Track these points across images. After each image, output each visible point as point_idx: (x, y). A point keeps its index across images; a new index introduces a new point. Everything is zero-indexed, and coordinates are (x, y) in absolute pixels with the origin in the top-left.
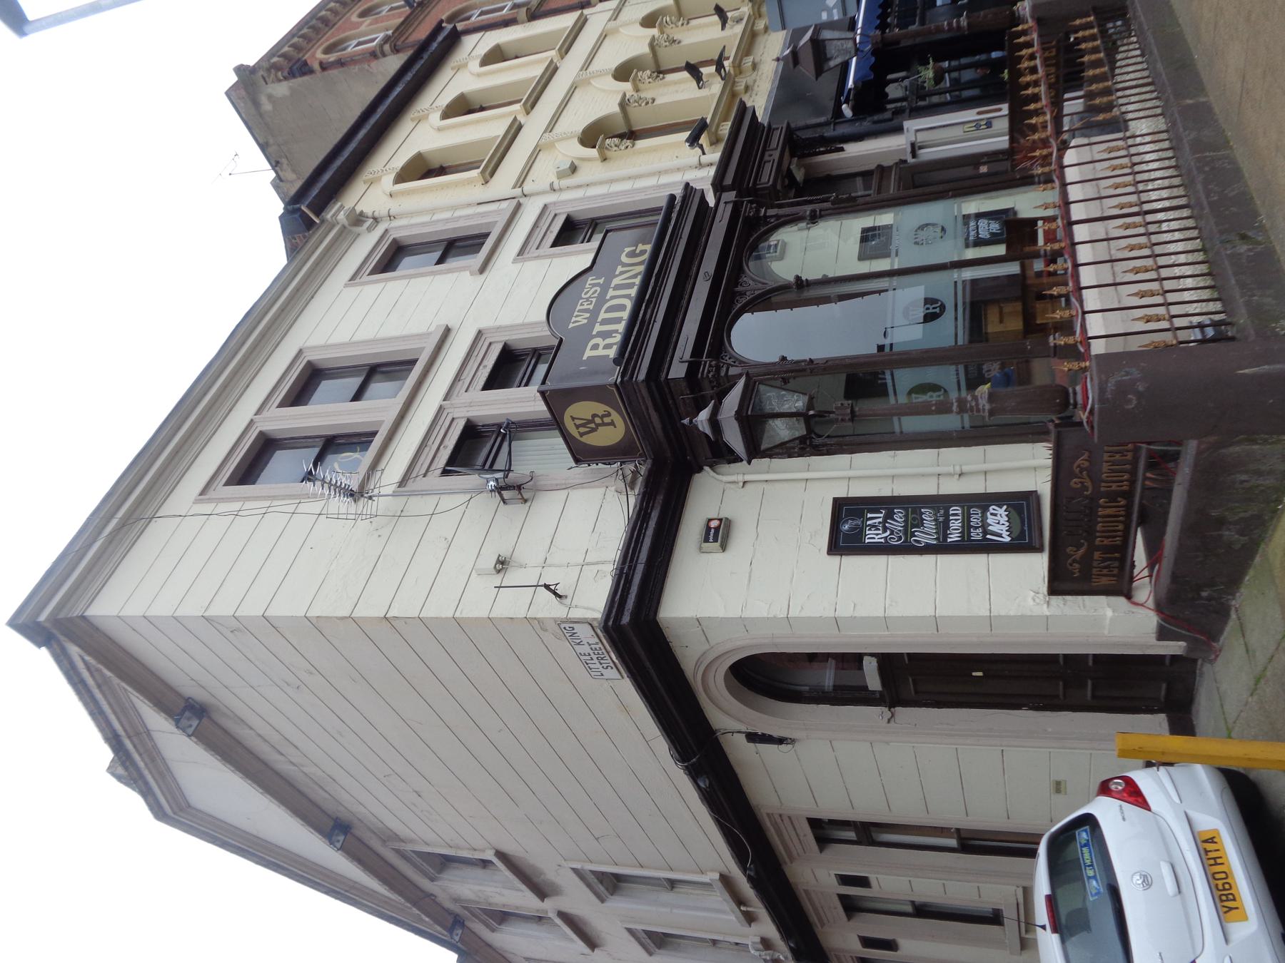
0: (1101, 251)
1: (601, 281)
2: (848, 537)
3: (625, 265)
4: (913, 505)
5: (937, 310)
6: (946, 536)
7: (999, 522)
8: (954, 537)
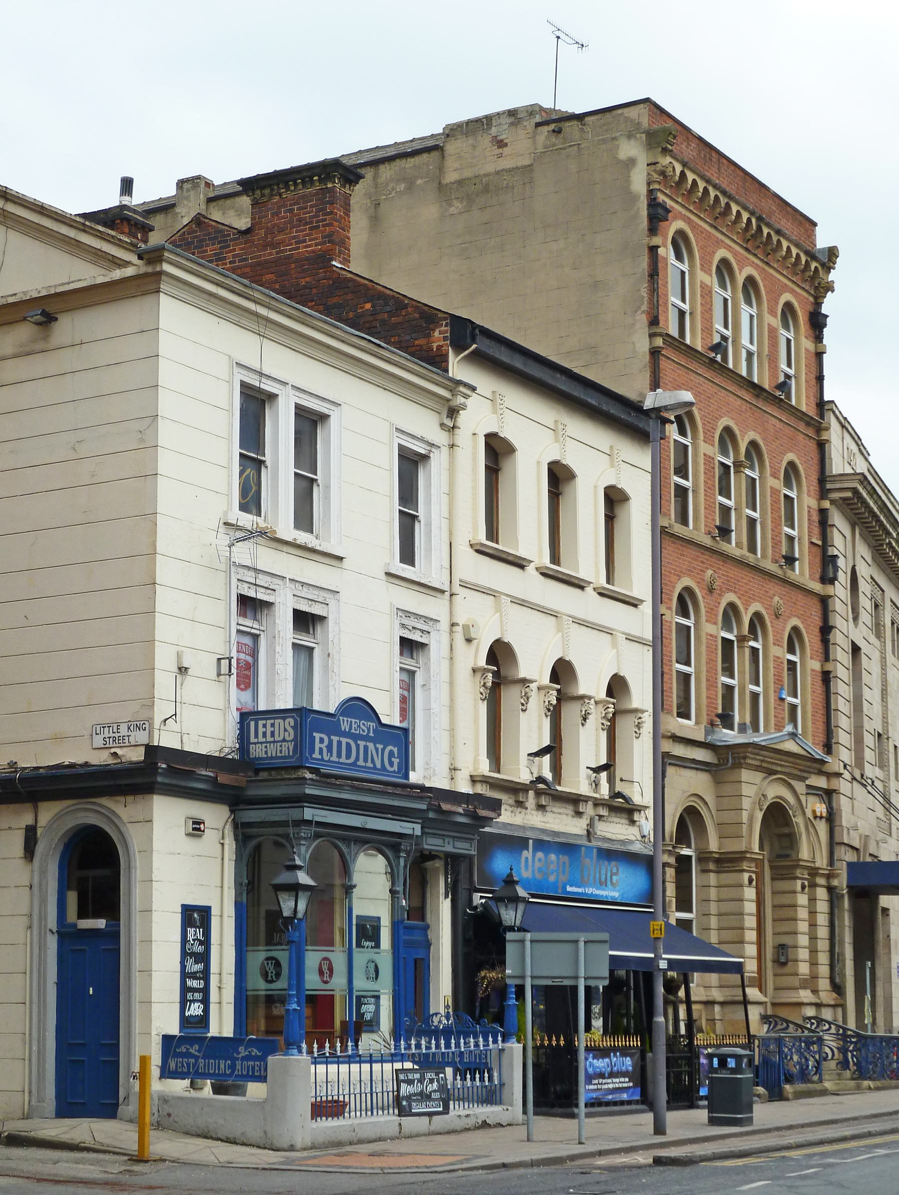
0: (355, 1077)
1: (371, 734)
2: (191, 916)
3: (383, 750)
4: (204, 958)
5: (269, 978)
6: (189, 978)
7: (195, 1010)
8: (189, 983)
